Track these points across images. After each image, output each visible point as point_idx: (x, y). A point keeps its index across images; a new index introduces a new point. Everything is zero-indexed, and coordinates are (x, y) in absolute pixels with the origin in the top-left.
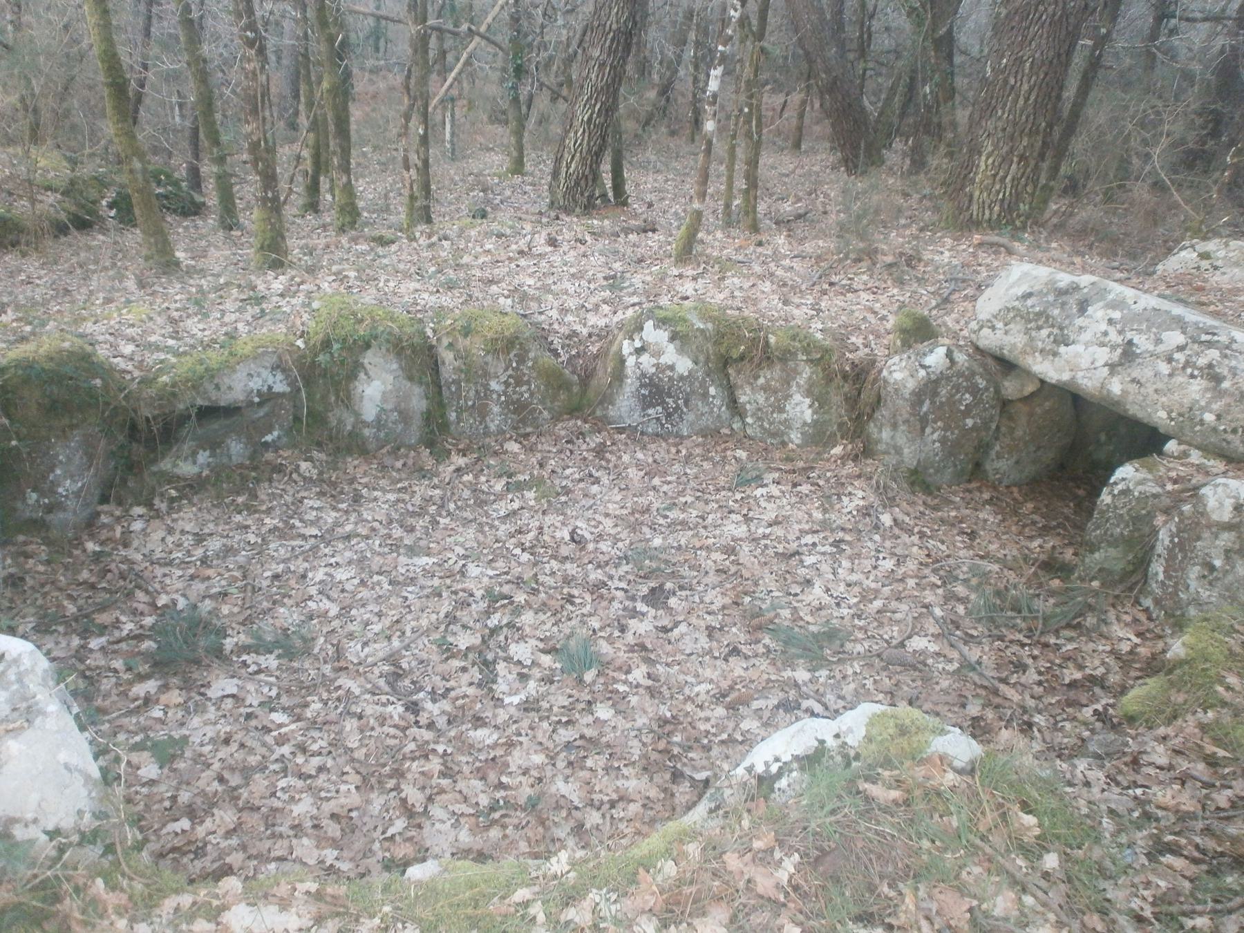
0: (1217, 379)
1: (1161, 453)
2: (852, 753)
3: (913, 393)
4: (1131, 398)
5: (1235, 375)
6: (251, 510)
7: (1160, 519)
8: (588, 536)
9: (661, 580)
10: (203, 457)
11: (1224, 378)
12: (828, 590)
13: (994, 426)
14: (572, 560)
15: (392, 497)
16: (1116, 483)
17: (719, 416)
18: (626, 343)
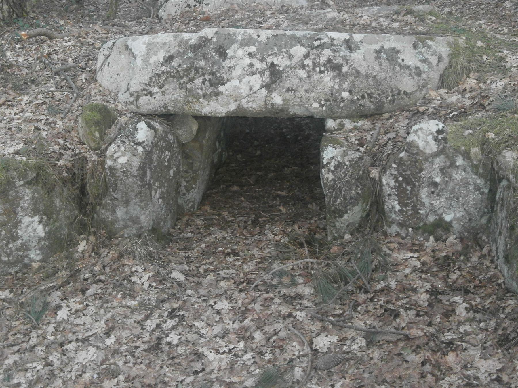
0: (337, 68)
11: (342, 65)
16: (328, 163)
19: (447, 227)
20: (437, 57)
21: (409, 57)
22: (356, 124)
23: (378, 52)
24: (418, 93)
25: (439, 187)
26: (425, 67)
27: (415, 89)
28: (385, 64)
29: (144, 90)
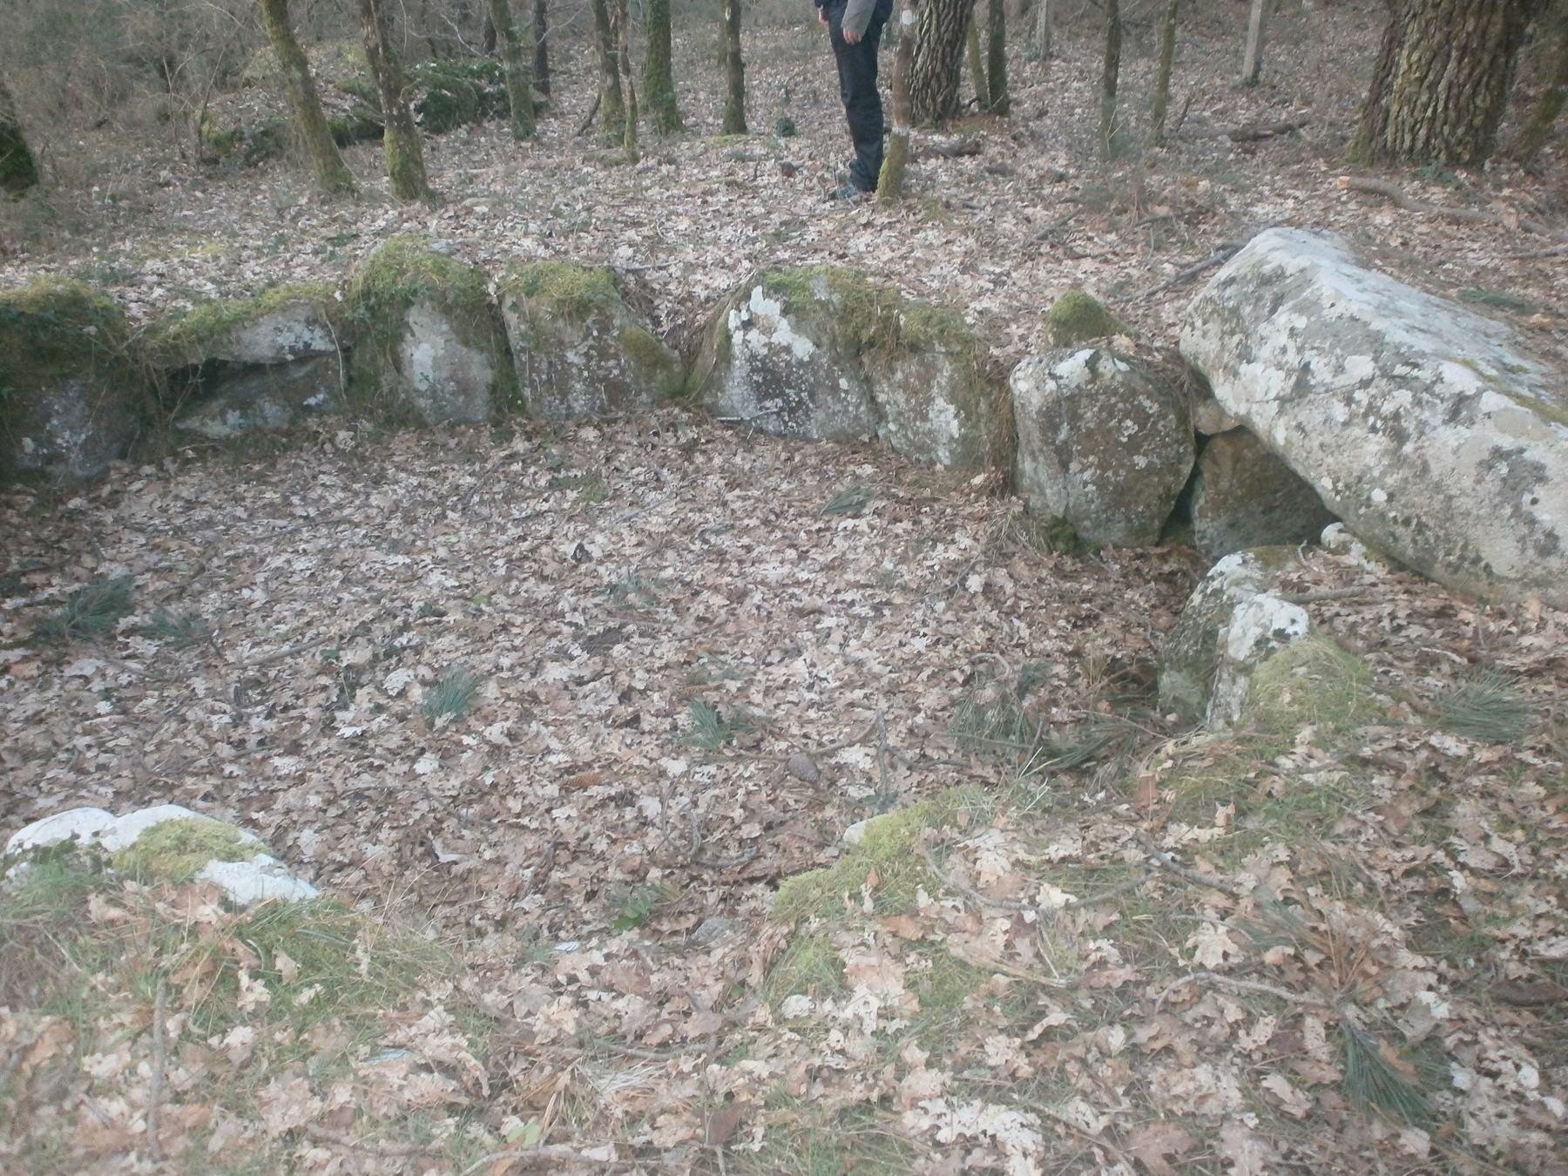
0: (1399, 436)
2: (104, 857)
6: (261, 479)
10: (233, 417)
15: (414, 481)
17: (857, 417)
23: (1498, 454)
24: (1517, 588)
27: (1513, 575)
28: (1491, 484)
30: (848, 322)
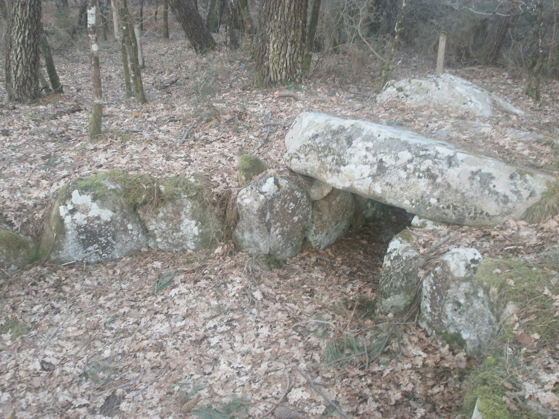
0: (433, 177)
1: (409, 224)
3: (258, 210)
4: (388, 195)
5: (443, 174)
7: (421, 273)
8: (54, 361)
9: (113, 388)
11: (437, 176)
12: (230, 364)
13: (310, 217)
14: (44, 389)
16: (391, 252)
17: (138, 241)
18: (62, 208)
19: (462, 343)
20: (529, 192)
21: (502, 185)
22: (436, 227)
23: (474, 174)
24: (500, 218)
25: (461, 308)
26: (513, 198)
27: (498, 214)
28: (476, 185)
29: (295, 154)
30: (128, 196)
